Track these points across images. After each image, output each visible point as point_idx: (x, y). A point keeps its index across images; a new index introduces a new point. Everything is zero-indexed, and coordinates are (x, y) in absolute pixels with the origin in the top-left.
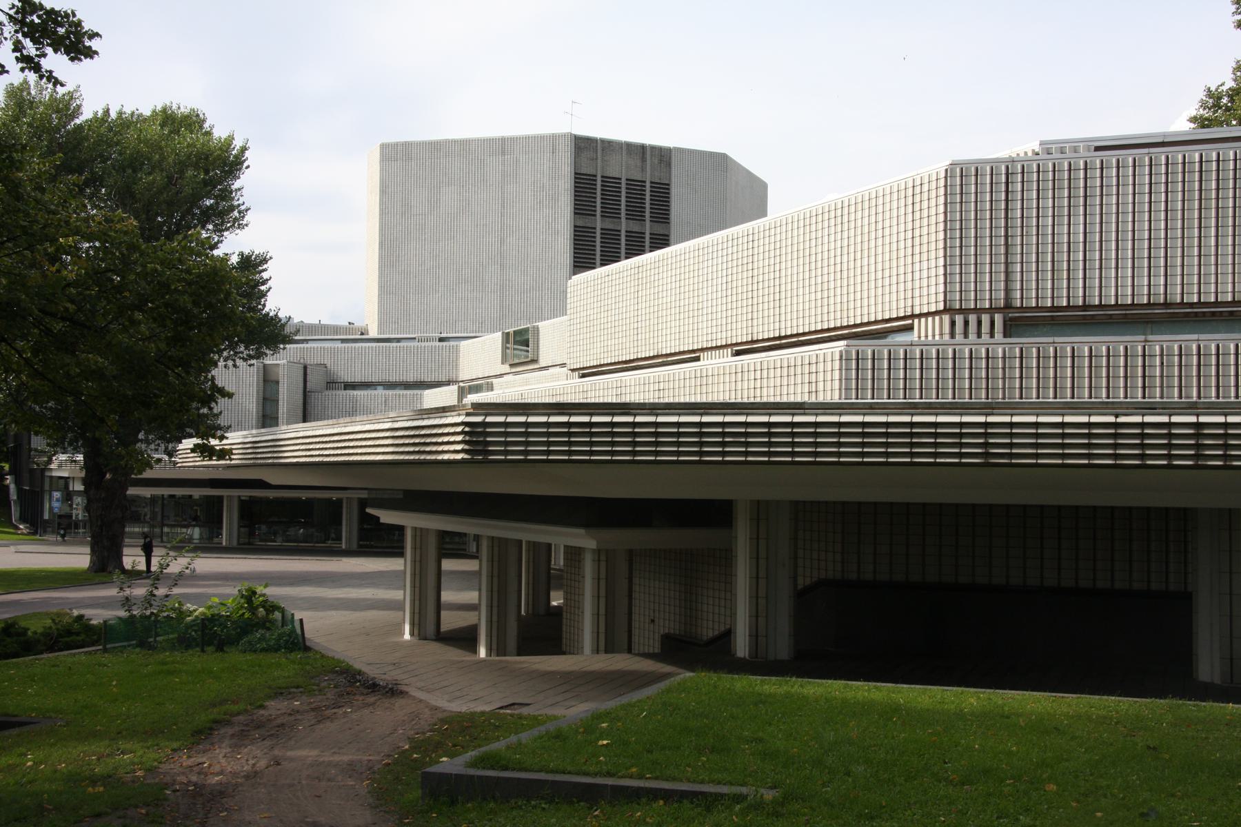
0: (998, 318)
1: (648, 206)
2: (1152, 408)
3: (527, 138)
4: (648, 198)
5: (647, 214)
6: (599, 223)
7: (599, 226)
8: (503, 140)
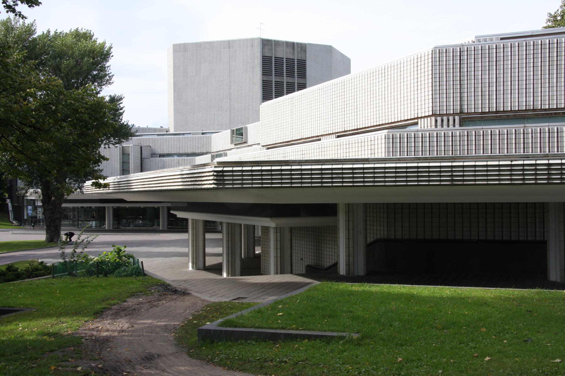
0: (457, 118)
1: (296, 70)
2: (527, 157)
4: (296, 67)
5: (296, 74)
6: (274, 79)
8: (229, 41)
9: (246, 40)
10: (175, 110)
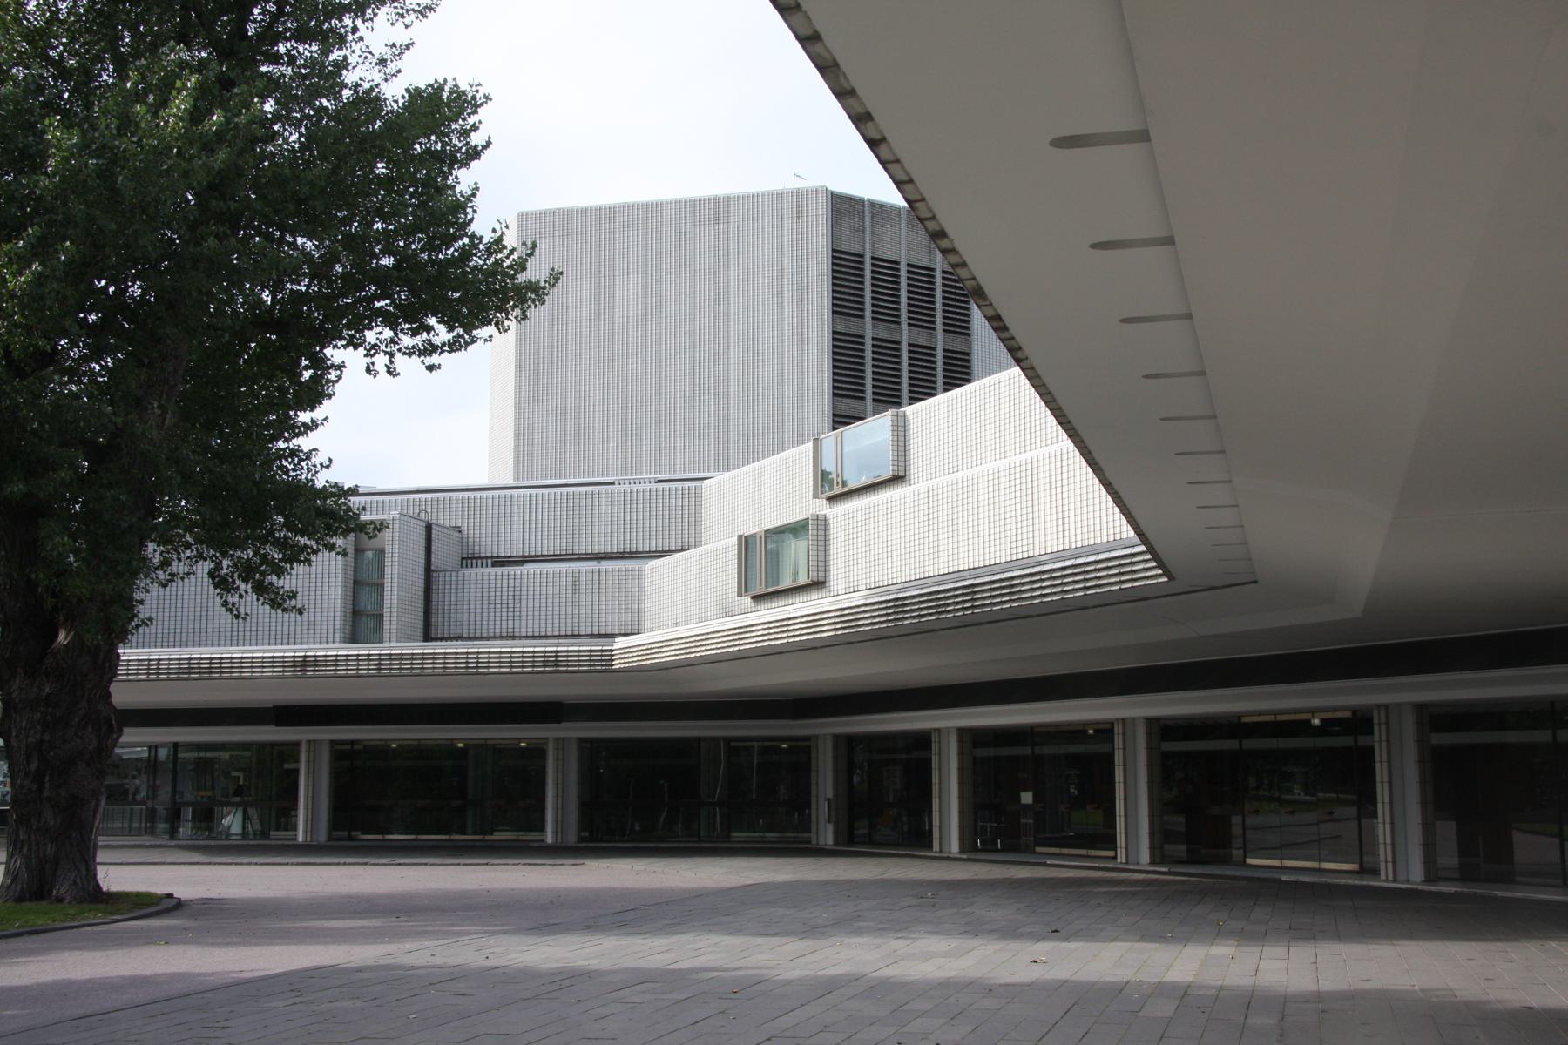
1: (939, 306)
3: (755, 197)
4: (939, 294)
5: (939, 320)
6: (869, 330)
7: (869, 334)
8: (716, 200)
9: (774, 199)
10: (519, 434)
